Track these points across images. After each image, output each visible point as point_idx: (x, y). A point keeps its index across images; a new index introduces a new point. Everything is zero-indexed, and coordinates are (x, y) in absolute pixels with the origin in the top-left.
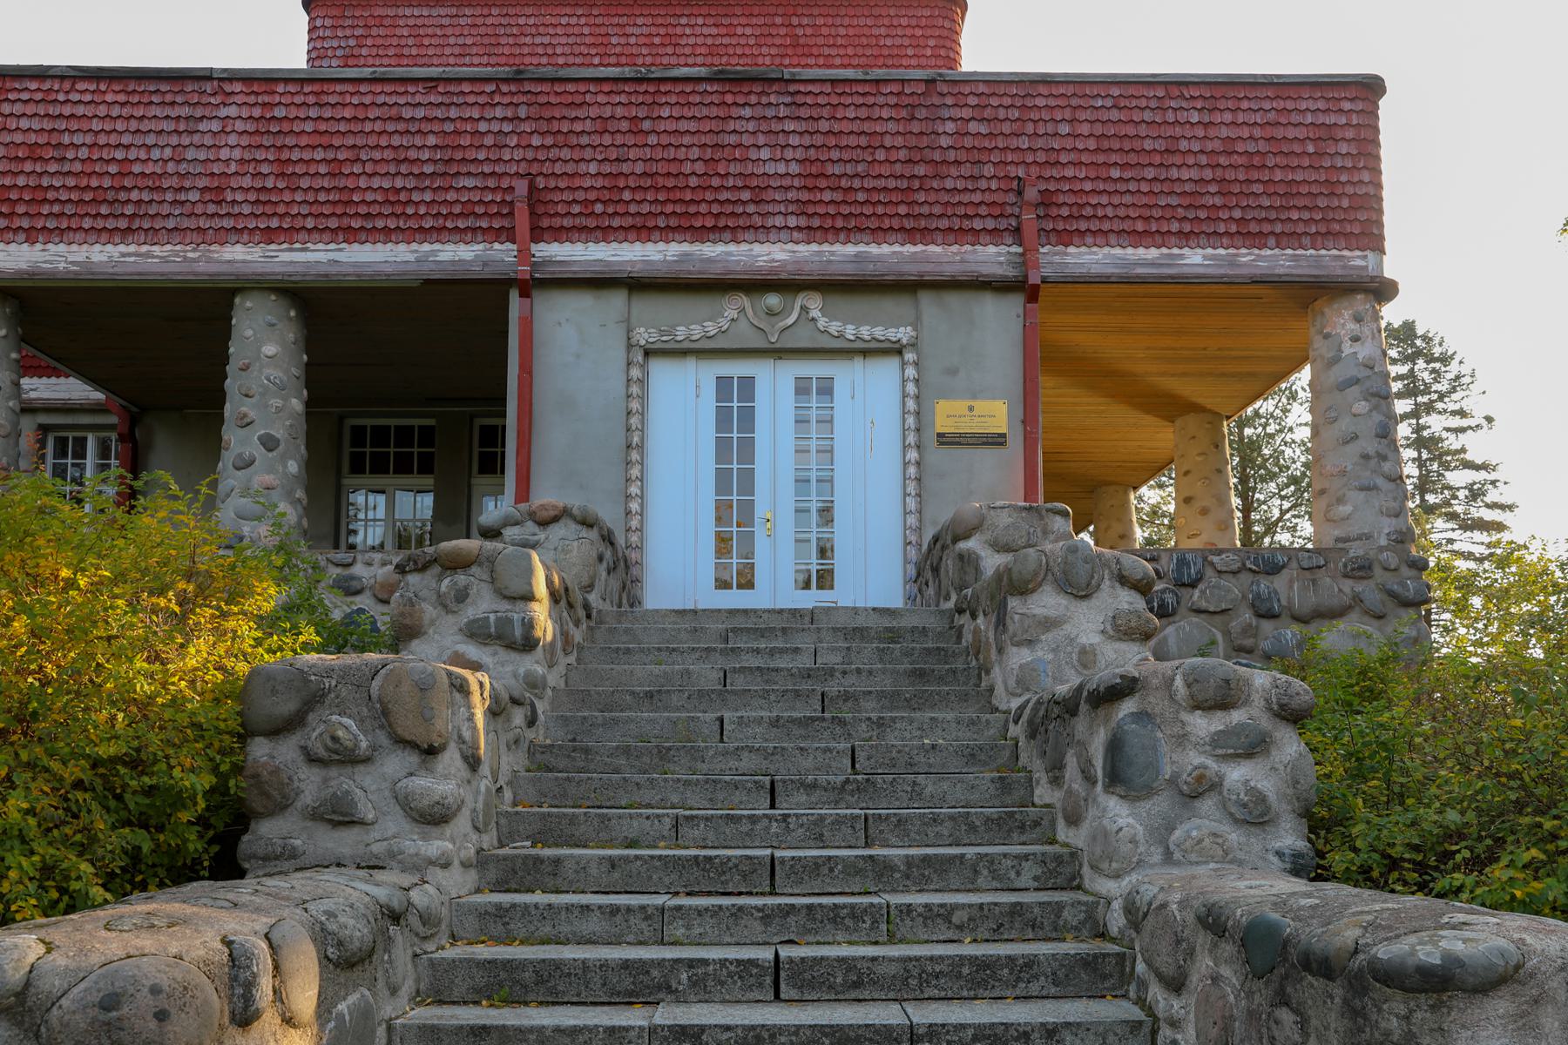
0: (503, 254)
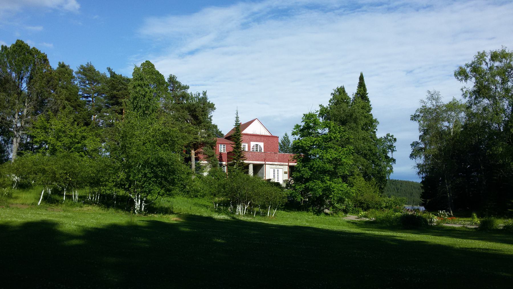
0: (264, 162)
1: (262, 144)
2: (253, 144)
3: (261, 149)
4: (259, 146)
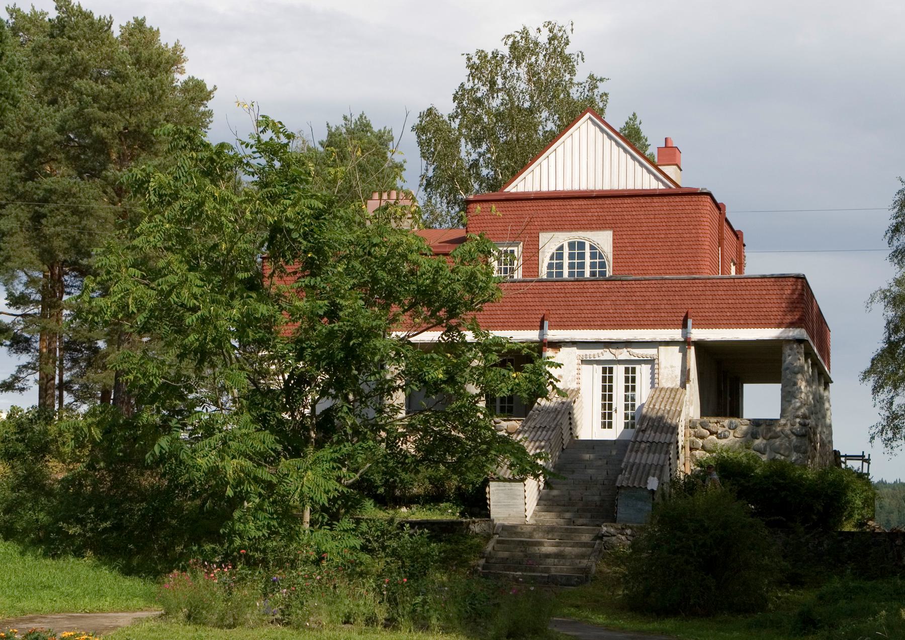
1: (604, 240)
3: (602, 265)
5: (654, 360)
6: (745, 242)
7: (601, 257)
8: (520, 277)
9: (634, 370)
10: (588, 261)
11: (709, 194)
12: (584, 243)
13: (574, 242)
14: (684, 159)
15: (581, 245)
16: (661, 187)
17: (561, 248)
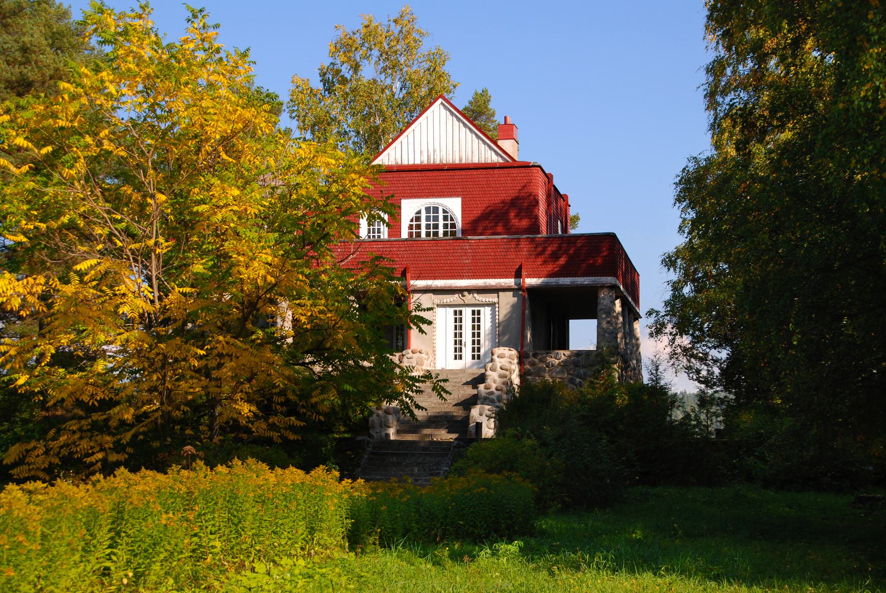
1: (454, 205)
2: (410, 208)
4: (441, 215)
5: (495, 303)
6: (570, 202)
7: (452, 219)
8: (386, 237)
9: (479, 312)
10: (441, 223)
11: (540, 167)
12: (438, 208)
13: (430, 207)
14: (518, 134)
15: (436, 210)
16: (501, 161)
17: (419, 212)
